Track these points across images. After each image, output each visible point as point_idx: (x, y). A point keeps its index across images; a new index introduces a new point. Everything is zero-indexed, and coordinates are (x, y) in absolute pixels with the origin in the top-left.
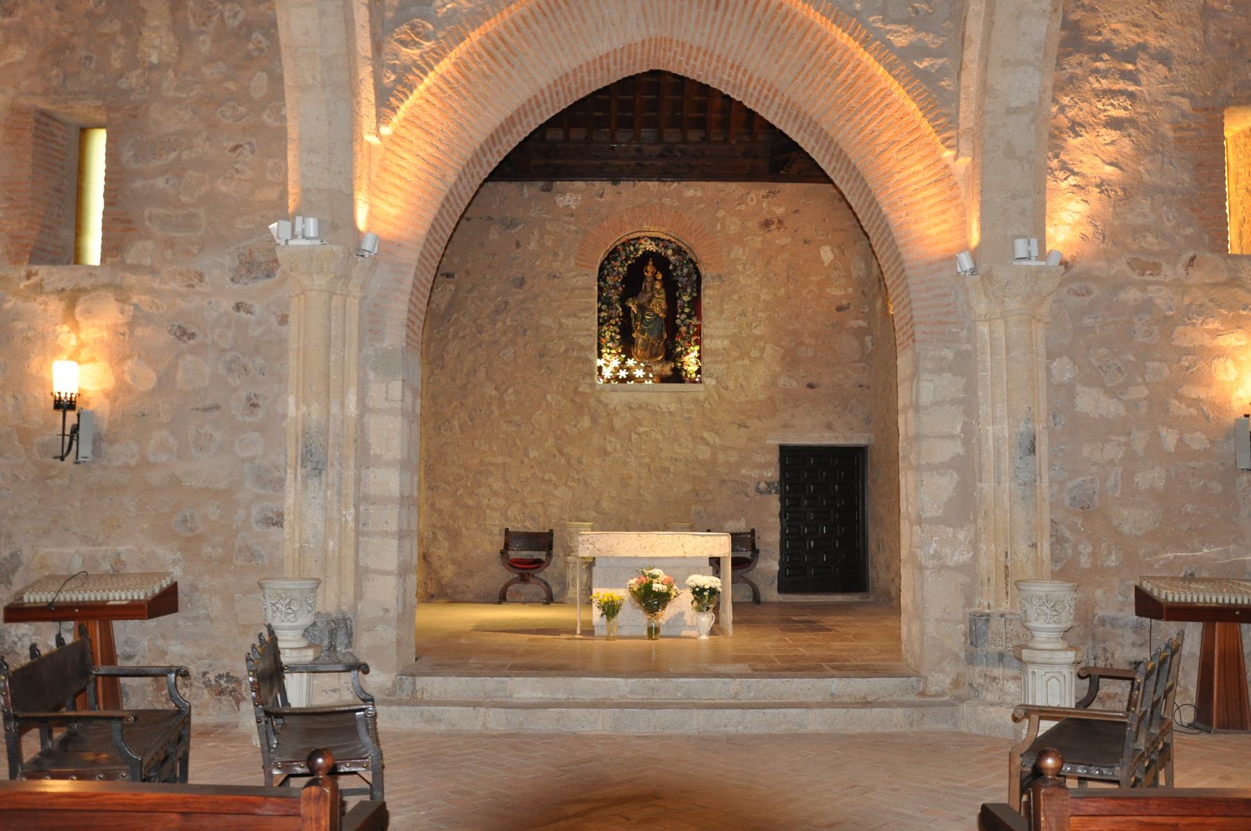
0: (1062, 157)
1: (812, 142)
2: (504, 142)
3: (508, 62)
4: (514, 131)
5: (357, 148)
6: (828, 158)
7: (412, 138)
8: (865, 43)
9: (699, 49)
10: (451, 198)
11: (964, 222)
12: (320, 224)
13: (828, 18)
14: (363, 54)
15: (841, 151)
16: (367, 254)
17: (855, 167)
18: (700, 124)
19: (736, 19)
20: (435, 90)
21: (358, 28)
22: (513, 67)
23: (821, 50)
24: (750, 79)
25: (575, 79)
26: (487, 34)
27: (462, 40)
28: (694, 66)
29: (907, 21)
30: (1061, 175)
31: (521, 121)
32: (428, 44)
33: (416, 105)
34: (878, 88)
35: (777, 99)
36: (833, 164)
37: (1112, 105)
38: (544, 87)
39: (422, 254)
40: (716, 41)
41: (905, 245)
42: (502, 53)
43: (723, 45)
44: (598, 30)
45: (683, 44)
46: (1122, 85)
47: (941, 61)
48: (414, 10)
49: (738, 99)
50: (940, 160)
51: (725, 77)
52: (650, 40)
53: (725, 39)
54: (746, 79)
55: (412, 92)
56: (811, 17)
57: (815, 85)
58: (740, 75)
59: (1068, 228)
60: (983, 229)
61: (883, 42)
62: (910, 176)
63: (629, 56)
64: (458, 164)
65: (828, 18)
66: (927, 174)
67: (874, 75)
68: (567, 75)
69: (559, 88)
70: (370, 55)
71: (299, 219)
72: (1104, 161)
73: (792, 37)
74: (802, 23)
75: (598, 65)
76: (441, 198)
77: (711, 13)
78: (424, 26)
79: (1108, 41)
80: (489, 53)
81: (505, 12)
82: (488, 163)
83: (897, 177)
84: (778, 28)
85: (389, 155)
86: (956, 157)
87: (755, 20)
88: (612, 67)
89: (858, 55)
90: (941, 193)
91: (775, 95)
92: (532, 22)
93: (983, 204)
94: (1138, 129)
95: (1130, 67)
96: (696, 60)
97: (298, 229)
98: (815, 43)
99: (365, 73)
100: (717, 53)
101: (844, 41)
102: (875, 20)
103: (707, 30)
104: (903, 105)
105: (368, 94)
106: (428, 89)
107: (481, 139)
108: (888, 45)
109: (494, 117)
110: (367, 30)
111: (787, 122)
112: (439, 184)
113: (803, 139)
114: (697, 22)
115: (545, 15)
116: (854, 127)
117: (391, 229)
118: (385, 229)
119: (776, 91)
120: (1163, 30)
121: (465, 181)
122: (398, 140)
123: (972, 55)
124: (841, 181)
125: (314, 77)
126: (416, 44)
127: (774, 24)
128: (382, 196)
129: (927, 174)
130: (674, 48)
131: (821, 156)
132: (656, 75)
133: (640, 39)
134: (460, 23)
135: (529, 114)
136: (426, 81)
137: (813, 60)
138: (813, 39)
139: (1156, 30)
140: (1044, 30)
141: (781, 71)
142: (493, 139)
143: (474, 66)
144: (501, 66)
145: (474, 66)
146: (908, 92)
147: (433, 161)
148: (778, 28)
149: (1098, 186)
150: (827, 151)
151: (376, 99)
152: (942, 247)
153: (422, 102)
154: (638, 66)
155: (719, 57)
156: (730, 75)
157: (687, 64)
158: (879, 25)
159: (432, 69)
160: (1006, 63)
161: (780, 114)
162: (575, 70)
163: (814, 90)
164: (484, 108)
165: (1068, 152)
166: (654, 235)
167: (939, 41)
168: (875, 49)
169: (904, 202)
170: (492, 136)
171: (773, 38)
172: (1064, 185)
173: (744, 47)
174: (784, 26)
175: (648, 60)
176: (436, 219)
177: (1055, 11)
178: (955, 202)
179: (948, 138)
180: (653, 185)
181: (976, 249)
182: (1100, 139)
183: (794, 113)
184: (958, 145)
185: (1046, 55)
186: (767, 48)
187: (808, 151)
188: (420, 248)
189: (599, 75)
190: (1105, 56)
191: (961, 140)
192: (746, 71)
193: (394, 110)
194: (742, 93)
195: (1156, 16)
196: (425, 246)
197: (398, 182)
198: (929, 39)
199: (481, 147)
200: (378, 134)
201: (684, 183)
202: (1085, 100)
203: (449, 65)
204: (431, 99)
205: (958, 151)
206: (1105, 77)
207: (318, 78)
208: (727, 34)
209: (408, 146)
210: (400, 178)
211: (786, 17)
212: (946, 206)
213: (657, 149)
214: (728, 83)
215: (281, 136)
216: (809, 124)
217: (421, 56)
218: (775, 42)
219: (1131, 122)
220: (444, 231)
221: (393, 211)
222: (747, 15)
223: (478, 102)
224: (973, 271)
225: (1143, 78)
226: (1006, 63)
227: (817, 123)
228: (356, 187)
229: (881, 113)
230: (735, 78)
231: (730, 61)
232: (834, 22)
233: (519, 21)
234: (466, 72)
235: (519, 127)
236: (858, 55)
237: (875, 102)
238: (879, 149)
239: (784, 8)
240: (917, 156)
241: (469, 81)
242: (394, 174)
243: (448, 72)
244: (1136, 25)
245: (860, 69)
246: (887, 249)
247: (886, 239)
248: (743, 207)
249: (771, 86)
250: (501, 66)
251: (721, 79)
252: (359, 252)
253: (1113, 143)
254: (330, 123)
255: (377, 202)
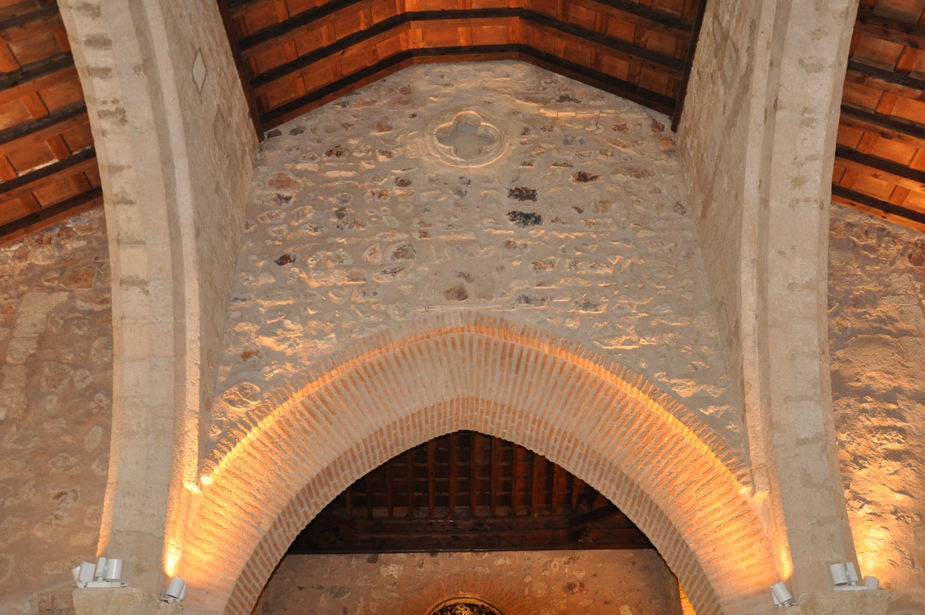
0: (852, 487)
1: (613, 488)
2: (321, 493)
3: (327, 419)
4: (331, 484)
5: (174, 493)
6: (629, 503)
7: (232, 488)
8: (654, 395)
9: (503, 406)
10: (265, 546)
11: (771, 555)
12: (124, 567)
13: (618, 375)
14: (191, 408)
15: (643, 492)
16: (171, 600)
17: (657, 507)
18: (507, 501)
19: (535, 380)
20: (258, 444)
21: (188, 385)
22: (331, 423)
23: (614, 404)
24: (551, 431)
25: (390, 436)
26: (309, 396)
27: (286, 400)
28: (499, 424)
29: (689, 376)
30: (856, 504)
31: (337, 474)
32: (254, 403)
33: (239, 458)
34: (670, 435)
35: (578, 449)
36: (635, 507)
37: (885, 439)
38: (360, 441)
39: (230, 601)
40: (518, 399)
41: (716, 581)
42: (322, 412)
43: (525, 402)
44: (410, 392)
45: (488, 403)
46: (890, 422)
47: (724, 408)
48: (245, 374)
49: (541, 454)
50: (737, 497)
51: (528, 433)
52: (458, 400)
53: (527, 397)
54: (547, 432)
55: (235, 445)
56: (602, 377)
57: (611, 433)
58: (542, 429)
59: (874, 555)
60: (794, 558)
61: (670, 394)
62: (711, 513)
63: (439, 415)
64: (274, 512)
65: (618, 375)
66: (728, 511)
67: (665, 424)
68: (381, 430)
69: (375, 443)
70: (197, 409)
71: (102, 561)
72: (892, 490)
73: (587, 393)
74: (594, 381)
75: (410, 423)
76: (255, 545)
77: (513, 375)
78: (252, 388)
79: (868, 386)
80: (310, 412)
81: (326, 376)
82: (305, 513)
83: (699, 515)
84: (573, 387)
85: (208, 503)
86: (753, 493)
87: (552, 381)
88: (424, 426)
89: (648, 407)
90: (744, 528)
91: (575, 445)
92: (351, 385)
93: (790, 533)
94: (915, 459)
95: (893, 406)
96: (500, 417)
97: (100, 570)
98: (608, 398)
99: (191, 426)
100: (519, 409)
101: (634, 396)
102: (660, 376)
103: (509, 390)
104: (695, 449)
105: (191, 445)
106: (251, 444)
107: (298, 489)
108: (675, 396)
109: (311, 469)
110: (197, 387)
111: (587, 473)
112: (254, 532)
113: (603, 487)
114: (500, 384)
115: (362, 379)
116: (652, 470)
117: (201, 575)
118: (195, 576)
119: (577, 440)
120: (912, 376)
121: (280, 530)
122: (218, 489)
123: (753, 398)
124: (644, 525)
125: (138, 424)
126: (243, 403)
127: (570, 384)
128: (197, 543)
129: (728, 511)
130: (480, 408)
131: (622, 501)
132: (466, 438)
133: (449, 399)
134: (285, 385)
135: (346, 467)
136: (250, 435)
137: (608, 412)
138: (606, 394)
139: (907, 376)
140: (817, 369)
141: (580, 423)
142: (310, 489)
143: (296, 424)
144: (321, 423)
145: (296, 424)
146: (699, 436)
147: (249, 510)
148: (573, 387)
149: (892, 513)
150: (628, 495)
151: (200, 449)
152: (753, 580)
153: (244, 455)
154: (447, 426)
155: (521, 412)
156: (532, 430)
157: (493, 423)
158: (664, 380)
159: (256, 425)
160: (788, 399)
161: (581, 465)
162: (388, 426)
163: (612, 438)
164: (303, 460)
165: (857, 483)
166: (468, 601)
167: (720, 391)
168: (664, 400)
169: (709, 539)
170: (308, 486)
171: (569, 395)
172: (861, 513)
173: (544, 403)
174: (579, 384)
175: (457, 420)
176: (248, 566)
177: (824, 353)
178: (759, 536)
179: (742, 476)
180: (467, 556)
181: (790, 579)
182: (884, 470)
183: (595, 461)
184: (753, 478)
185: (823, 391)
186: (566, 403)
187: (609, 498)
188: (229, 595)
189: (412, 434)
190: (869, 399)
191: (756, 476)
192: (547, 424)
193: (217, 461)
194: (544, 447)
195: (903, 365)
196: (234, 594)
197: (213, 530)
198: (710, 389)
199: (298, 496)
200: (198, 483)
201: (494, 553)
202: (861, 436)
203: (273, 423)
204: (253, 452)
205: (754, 486)
206: (873, 416)
207: (143, 425)
208: (528, 392)
209: (227, 495)
210: (216, 525)
211: (580, 378)
212: (751, 540)
213: (470, 523)
214: (530, 438)
215: (101, 484)
216: (609, 470)
217: (247, 414)
218: (572, 399)
219: (908, 453)
220: (257, 580)
221: (206, 558)
222: (544, 376)
223: (297, 455)
224: (791, 602)
225: (907, 416)
226: (788, 399)
227: (617, 468)
228: (169, 531)
229: (676, 456)
230: (537, 433)
231: (532, 416)
232: (623, 379)
233: (339, 385)
234: (288, 429)
235: (336, 480)
236: (648, 407)
237: (669, 447)
238: (678, 490)
239: (578, 370)
240: (715, 495)
241: (289, 436)
242: (211, 522)
243: (271, 428)
244: (888, 373)
245: (651, 419)
246: (698, 587)
247: (696, 577)
248: (548, 573)
249: (571, 437)
250: (321, 423)
251: (524, 435)
252: (164, 597)
253: (896, 472)
254: (148, 467)
255: (191, 549)
